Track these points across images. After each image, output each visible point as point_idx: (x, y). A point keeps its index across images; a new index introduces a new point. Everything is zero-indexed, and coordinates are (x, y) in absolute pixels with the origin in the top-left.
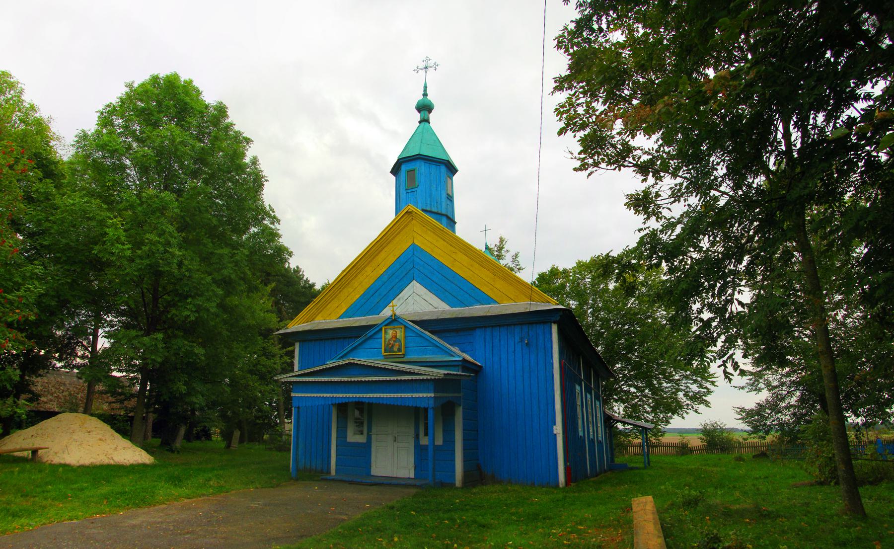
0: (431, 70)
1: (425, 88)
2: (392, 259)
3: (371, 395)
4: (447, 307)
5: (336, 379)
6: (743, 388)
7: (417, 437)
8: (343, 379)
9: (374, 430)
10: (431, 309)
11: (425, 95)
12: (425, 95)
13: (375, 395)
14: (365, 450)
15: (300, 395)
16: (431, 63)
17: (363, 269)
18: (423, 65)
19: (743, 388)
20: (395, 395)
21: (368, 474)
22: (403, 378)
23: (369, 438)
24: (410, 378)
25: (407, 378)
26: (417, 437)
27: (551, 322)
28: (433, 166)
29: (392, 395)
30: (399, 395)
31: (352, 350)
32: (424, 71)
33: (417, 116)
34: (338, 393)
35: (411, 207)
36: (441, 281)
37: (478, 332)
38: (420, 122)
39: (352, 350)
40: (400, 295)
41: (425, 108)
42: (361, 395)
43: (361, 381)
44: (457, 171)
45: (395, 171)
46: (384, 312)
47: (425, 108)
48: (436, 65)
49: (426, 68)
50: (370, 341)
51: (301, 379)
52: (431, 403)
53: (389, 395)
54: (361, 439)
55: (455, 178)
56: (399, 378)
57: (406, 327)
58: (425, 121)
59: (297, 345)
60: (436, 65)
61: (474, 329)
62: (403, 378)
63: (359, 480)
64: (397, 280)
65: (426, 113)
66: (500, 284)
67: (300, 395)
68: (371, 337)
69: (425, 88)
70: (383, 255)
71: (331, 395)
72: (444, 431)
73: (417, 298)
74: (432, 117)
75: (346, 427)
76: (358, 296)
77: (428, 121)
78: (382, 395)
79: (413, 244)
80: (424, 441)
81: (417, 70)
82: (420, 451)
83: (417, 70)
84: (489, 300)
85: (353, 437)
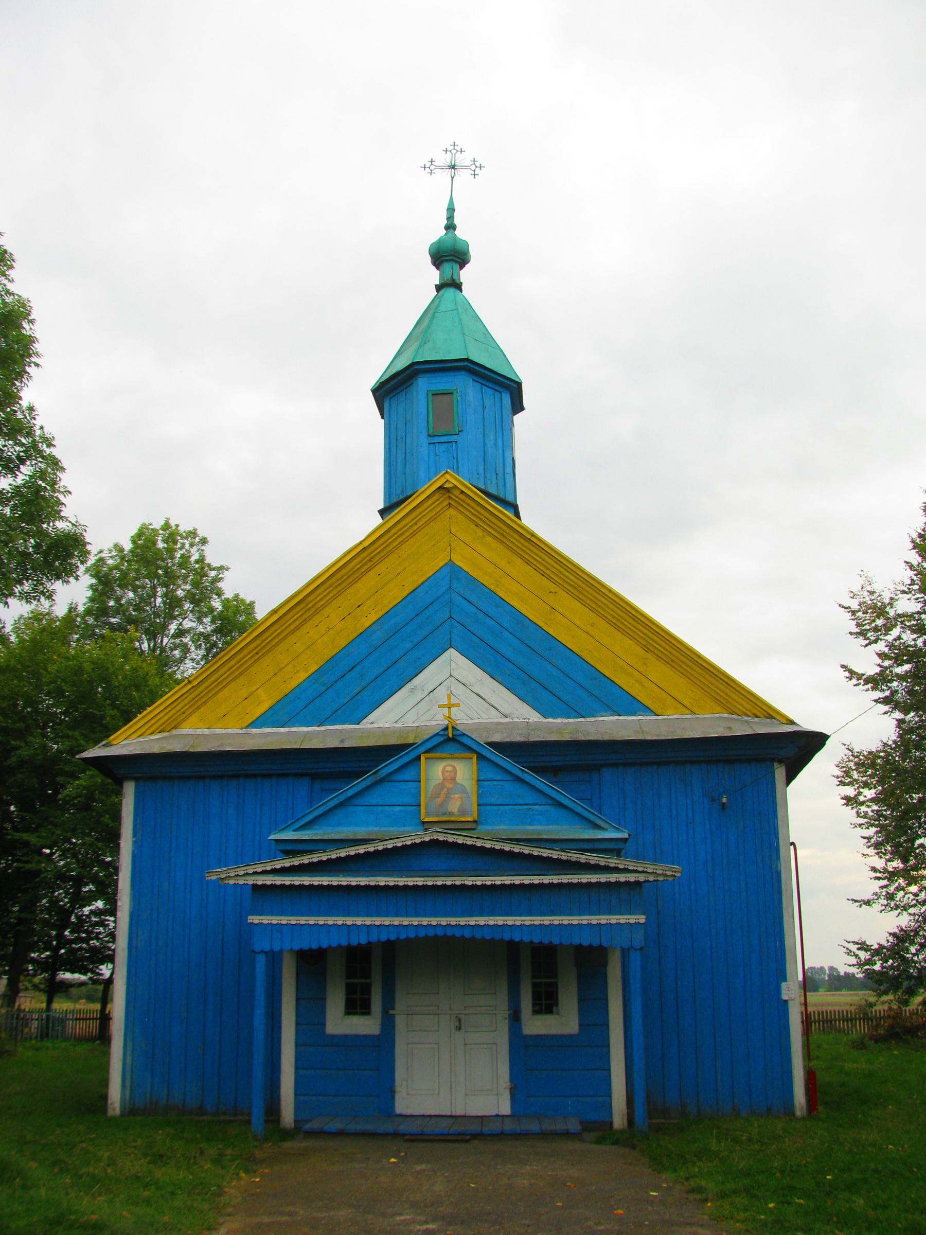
0: (463, 176)
1: (451, 210)
2: (395, 594)
3: (482, 921)
4: (534, 717)
5: (391, 881)
6: (868, 903)
7: (515, 1017)
8: (402, 881)
9: (401, 1003)
10: (493, 717)
11: (450, 227)
12: (450, 227)
13: (492, 921)
14: (379, 1053)
15: (266, 920)
16: (462, 160)
17: (317, 612)
18: (443, 159)
19: (868, 903)
20: (546, 920)
21: (387, 1109)
22: (575, 879)
23: (388, 1022)
24: (593, 878)
25: (585, 878)
26: (515, 1017)
27: (773, 760)
28: (490, 392)
29: (537, 920)
30: (557, 920)
31: (341, 805)
32: (448, 172)
33: (434, 276)
34: (492, 913)
35: (452, 479)
36: (516, 653)
37: (608, 775)
38: (439, 288)
39: (341, 805)
40: (416, 681)
41: (449, 256)
42: (453, 921)
43: (463, 887)
44: (522, 409)
45: (388, 391)
46: (372, 717)
47: (449, 256)
48: (476, 168)
49: (453, 167)
50: (387, 786)
51: (287, 880)
52: (638, 939)
53: (528, 920)
54: (365, 1026)
55: (517, 418)
56: (565, 879)
57: (481, 757)
58: (451, 284)
59: (129, 789)
60: (476, 168)
61: (598, 768)
62: (575, 879)
63: (360, 1127)
64: (408, 645)
65: (456, 267)
66: (658, 672)
67: (266, 920)
68: (387, 779)
69: (451, 210)
70: (370, 581)
71: (368, 921)
72: (580, 1000)
73: (459, 690)
74: (465, 275)
75: (321, 1001)
76: (303, 676)
77: (458, 286)
78: (510, 920)
79: (451, 563)
80: (536, 1025)
81: (430, 167)
82: (526, 1055)
83: (430, 167)
84: (631, 705)
85: (339, 1022)
